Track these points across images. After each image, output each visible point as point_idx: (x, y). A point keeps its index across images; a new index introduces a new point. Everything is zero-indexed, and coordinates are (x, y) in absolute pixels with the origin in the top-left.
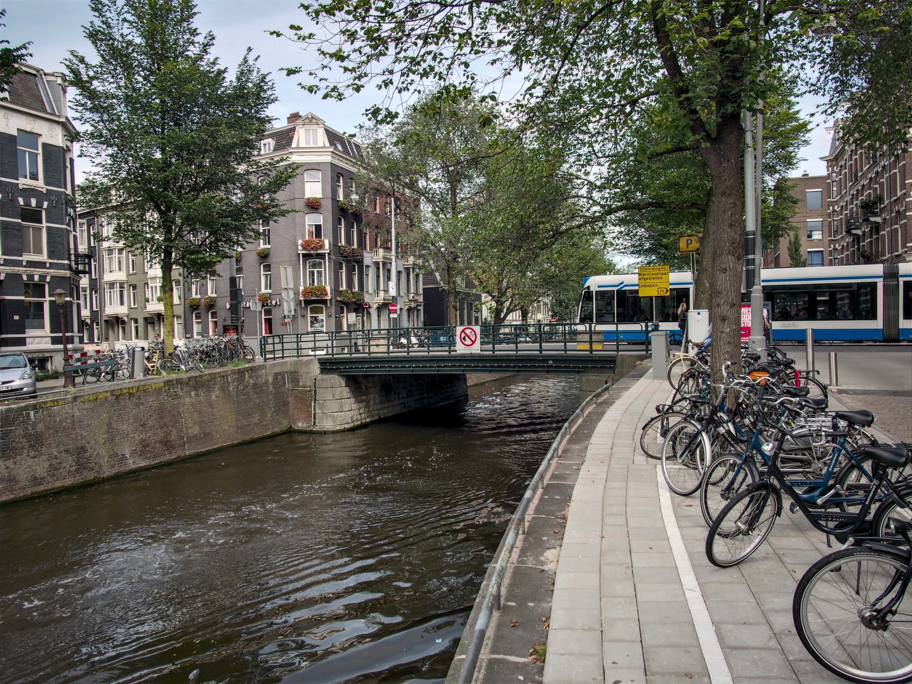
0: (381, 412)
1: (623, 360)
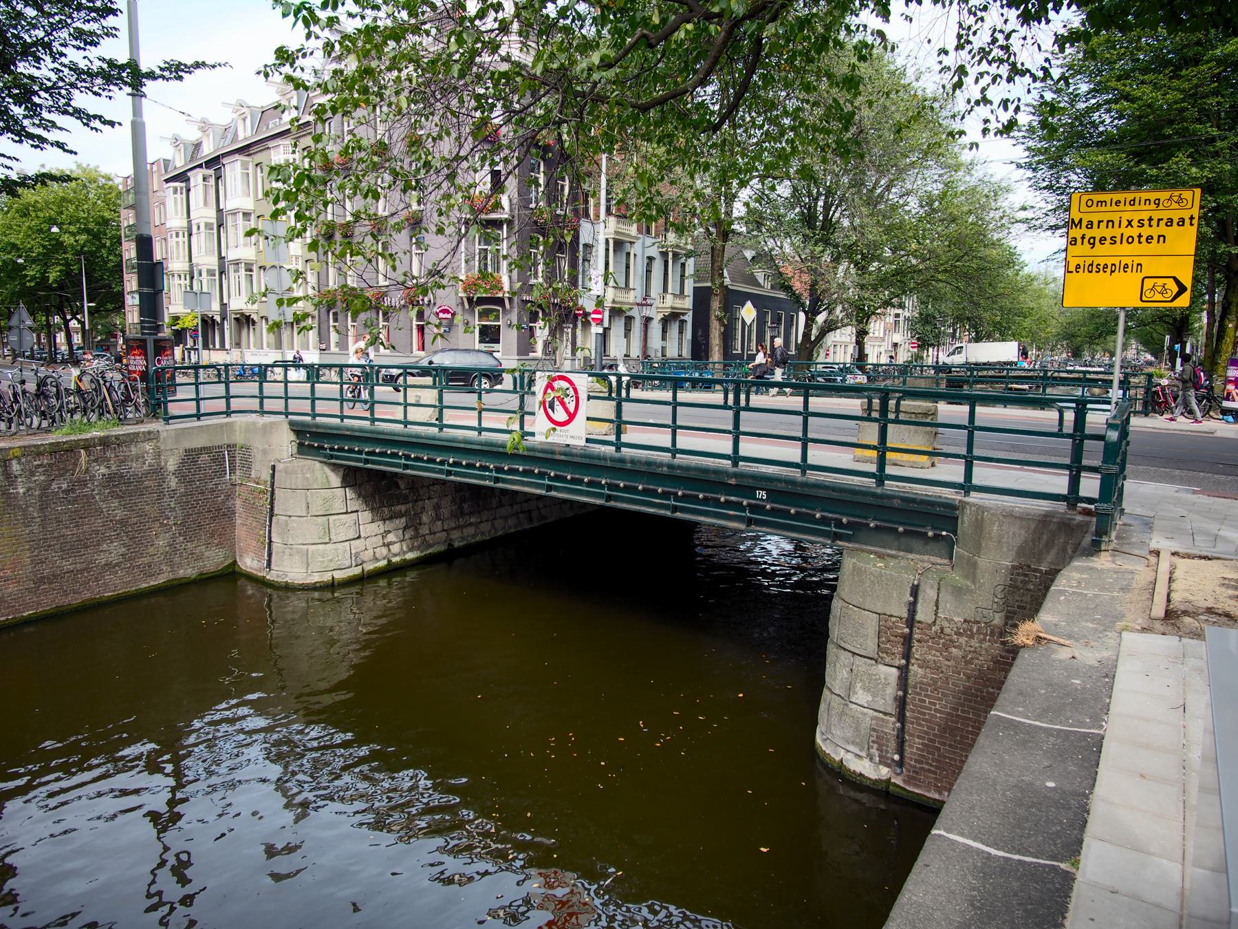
0: (455, 535)
1: (979, 525)
